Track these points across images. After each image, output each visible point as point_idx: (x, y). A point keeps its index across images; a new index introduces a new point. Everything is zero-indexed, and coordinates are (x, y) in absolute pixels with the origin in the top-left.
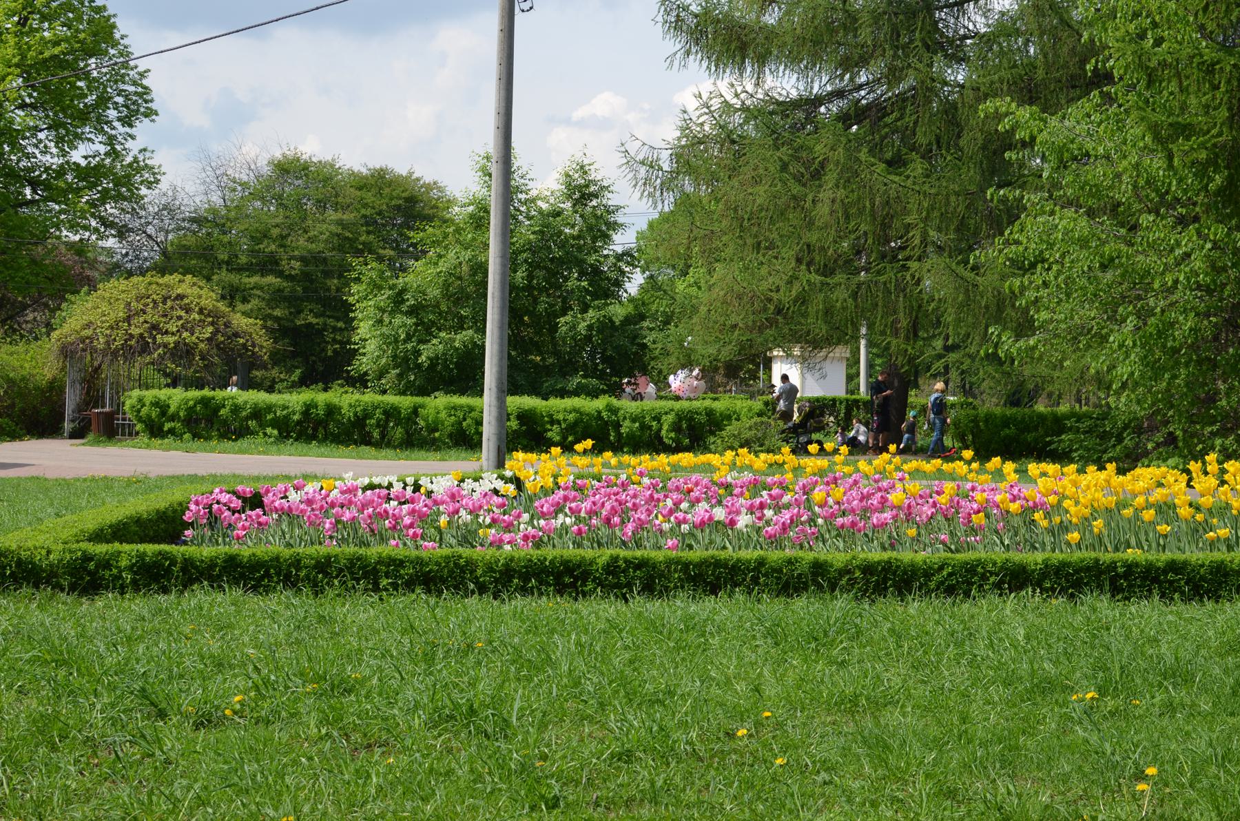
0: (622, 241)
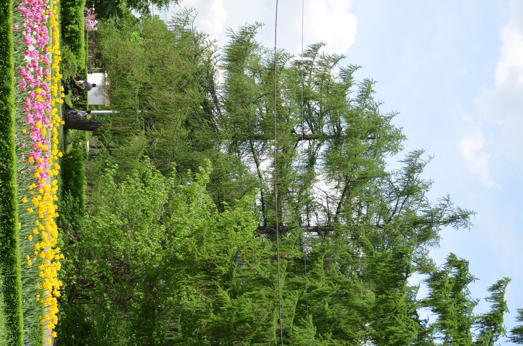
0: (153, 9)
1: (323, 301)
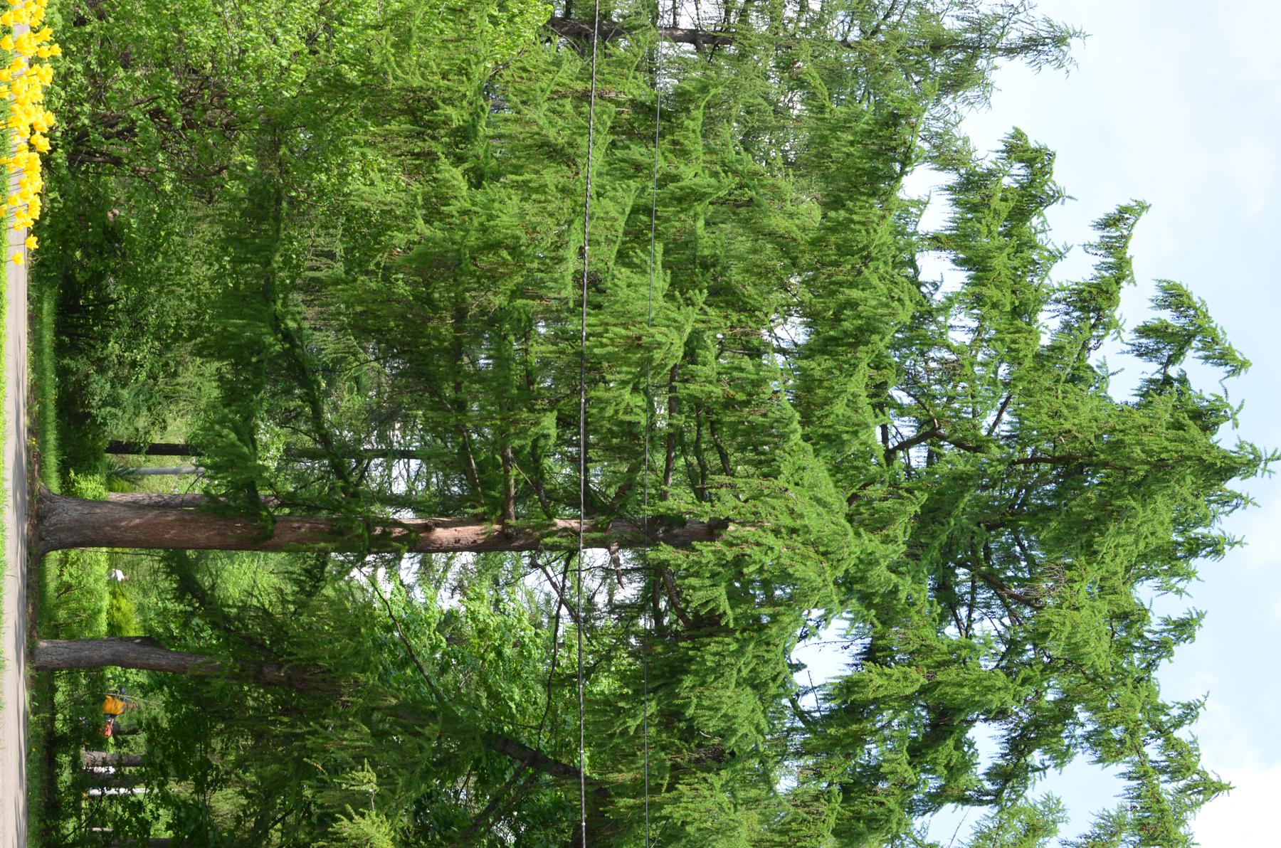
1: (692, 213)
